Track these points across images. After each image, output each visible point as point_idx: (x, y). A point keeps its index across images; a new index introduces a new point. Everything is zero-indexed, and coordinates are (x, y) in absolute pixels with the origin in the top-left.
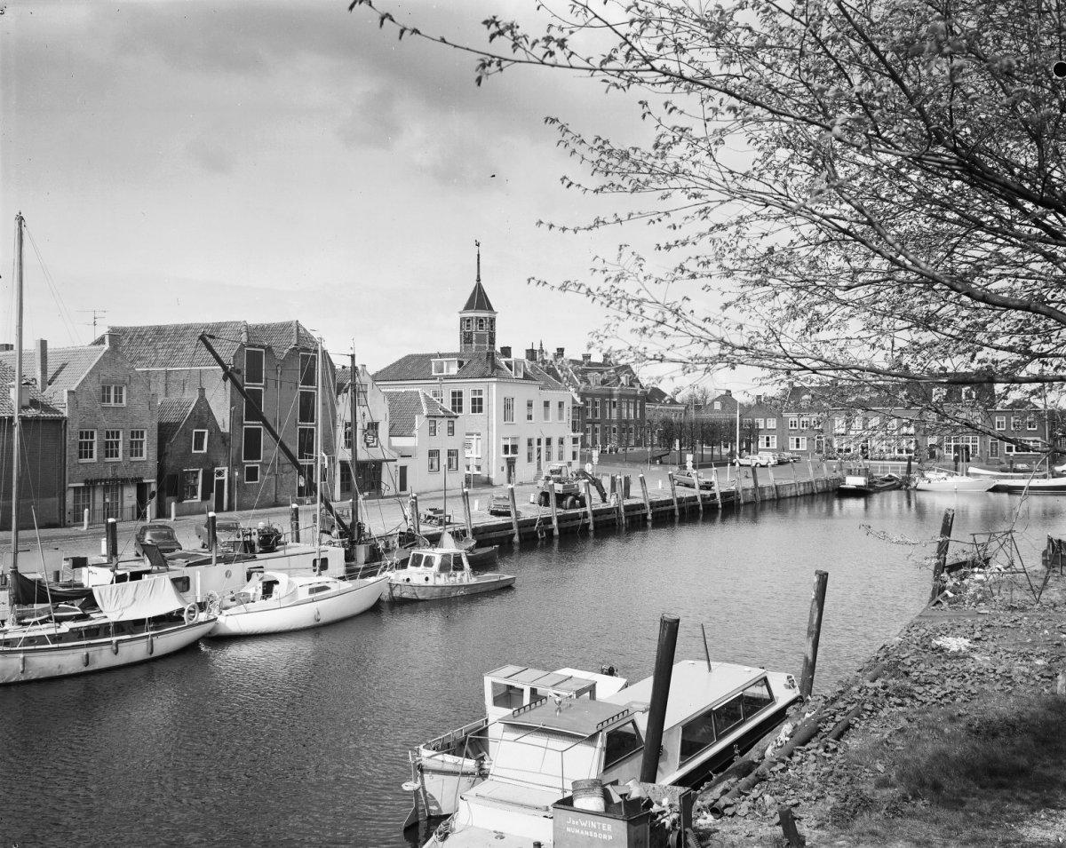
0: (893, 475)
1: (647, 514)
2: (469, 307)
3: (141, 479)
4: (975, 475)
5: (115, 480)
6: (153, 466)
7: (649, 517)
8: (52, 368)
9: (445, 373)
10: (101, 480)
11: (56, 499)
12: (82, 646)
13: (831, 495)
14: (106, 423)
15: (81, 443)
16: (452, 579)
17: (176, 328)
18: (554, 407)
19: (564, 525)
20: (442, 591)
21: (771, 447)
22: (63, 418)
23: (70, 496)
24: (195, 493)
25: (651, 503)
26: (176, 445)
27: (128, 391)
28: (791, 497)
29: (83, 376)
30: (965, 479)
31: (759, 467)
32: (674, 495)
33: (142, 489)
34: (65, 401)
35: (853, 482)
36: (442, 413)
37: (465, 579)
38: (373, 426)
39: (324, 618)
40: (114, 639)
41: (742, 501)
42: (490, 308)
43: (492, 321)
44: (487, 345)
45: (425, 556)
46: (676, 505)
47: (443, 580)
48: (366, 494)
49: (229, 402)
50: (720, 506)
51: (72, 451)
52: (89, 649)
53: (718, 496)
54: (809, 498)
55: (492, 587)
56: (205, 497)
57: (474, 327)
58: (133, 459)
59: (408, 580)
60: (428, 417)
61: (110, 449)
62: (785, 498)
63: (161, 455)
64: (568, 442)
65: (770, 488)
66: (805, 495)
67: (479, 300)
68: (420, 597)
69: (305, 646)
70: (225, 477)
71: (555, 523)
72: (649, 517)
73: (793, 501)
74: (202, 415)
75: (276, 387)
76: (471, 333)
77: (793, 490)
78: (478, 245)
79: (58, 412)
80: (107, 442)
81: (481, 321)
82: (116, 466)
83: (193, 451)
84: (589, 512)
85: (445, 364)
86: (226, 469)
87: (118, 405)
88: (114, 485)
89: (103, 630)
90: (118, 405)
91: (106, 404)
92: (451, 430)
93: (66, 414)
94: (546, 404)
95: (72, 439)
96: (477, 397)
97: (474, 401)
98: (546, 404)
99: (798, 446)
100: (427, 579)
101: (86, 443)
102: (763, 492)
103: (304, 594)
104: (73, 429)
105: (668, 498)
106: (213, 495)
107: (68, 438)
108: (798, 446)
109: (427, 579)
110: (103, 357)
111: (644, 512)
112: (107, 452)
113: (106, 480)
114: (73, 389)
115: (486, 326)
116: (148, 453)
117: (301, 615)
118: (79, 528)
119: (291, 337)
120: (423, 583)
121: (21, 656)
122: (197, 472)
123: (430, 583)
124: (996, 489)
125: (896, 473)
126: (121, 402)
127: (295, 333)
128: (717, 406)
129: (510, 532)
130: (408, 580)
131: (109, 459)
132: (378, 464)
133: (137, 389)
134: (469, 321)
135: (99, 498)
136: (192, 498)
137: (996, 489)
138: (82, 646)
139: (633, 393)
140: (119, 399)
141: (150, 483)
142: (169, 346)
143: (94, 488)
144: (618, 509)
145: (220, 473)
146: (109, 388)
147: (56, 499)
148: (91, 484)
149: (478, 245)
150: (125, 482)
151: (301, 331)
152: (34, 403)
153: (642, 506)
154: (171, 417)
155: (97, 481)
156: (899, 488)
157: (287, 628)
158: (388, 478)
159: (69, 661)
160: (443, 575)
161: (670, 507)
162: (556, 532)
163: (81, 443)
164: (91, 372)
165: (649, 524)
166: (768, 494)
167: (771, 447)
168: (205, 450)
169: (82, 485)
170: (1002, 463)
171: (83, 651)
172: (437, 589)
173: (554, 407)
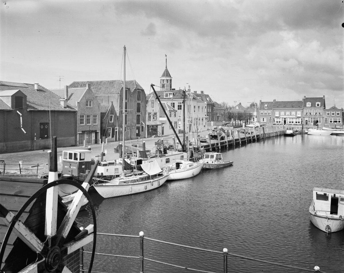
0: (298, 130)
1: (239, 142)
2: (163, 76)
3: (96, 131)
4: (325, 130)
5: (89, 131)
6: (99, 126)
7: (240, 143)
8: (69, 95)
9: (168, 97)
10: (86, 131)
11: (74, 137)
12: (144, 183)
13: (274, 137)
14: (87, 113)
15: (81, 119)
16: (219, 162)
17: (97, 82)
18: (197, 107)
19: (222, 145)
20: (217, 166)
21: (264, 121)
22: (77, 111)
23: (78, 136)
24: (109, 135)
25: (247, 137)
26: (106, 120)
27: (93, 102)
28: (272, 137)
29: (81, 98)
30: (323, 131)
31: (253, 128)
32: (239, 137)
33: (96, 133)
34: (77, 106)
35: (289, 132)
36: (173, 110)
37: (222, 162)
38: (155, 114)
39: (195, 174)
40: (152, 180)
41: (261, 138)
42: (170, 76)
43: (171, 80)
44: (169, 88)
45: (210, 155)
46: (246, 139)
47: (216, 163)
48: (155, 136)
49: (119, 106)
50: (256, 139)
51: (78, 122)
52: (146, 184)
53: (256, 136)
54: (276, 137)
55: (229, 165)
56: (113, 137)
57: (165, 82)
58: (94, 124)
59: (208, 162)
60: (169, 111)
61: (88, 121)
62: (271, 137)
63: (102, 123)
64: (204, 119)
65: (267, 134)
66: (275, 136)
67: (167, 73)
68: (211, 168)
69: (190, 182)
70: (118, 130)
71: (219, 145)
72: (240, 143)
73: (273, 138)
74: (112, 111)
75: (131, 101)
76: (164, 84)
77: (273, 135)
78: (166, 56)
79: (74, 109)
80: (87, 119)
81: (168, 80)
82: (90, 126)
83: (110, 122)
84: (227, 141)
85: (168, 94)
86: (118, 127)
87: (90, 107)
88: (90, 132)
89: (148, 178)
90: (90, 107)
91: (87, 107)
92: (175, 115)
93: (77, 110)
94: (199, 107)
95: (78, 118)
96: (180, 105)
97: (178, 106)
98: (199, 107)
99: (263, 120)
100: (213, 162)
101: (82, 119)
102: (265, 135)
103: (188, 167)
104: (79, 114)
105: (244, 137)
106: (115, 136)
107: (77, 117)
108: (263, 120)
109: (213, 162)
110: (87, 91)
111: (239, 141)
112: (81, 122)
113: (87, 131)
114: (79, 101)
115: (169, 82)
116: (98, 123)
117: (189, 174)
118: (82, 147)
119: (134, 85)
120: (211, 163)
121: (131, 186)
122: (110, 129)
123: (213, 163)
124: (332, 134)
125: (299, 129)
126: (91, 106)
127: (135, 84)
128: (237, 108)
129: (209, 147)
130: (208, 162)
131: (88, 124)
132: (157, 126)
133: (95, 101)
134: (163, 80)
135: (86, 137)
136: (109, 137)
137: (332, 134)
138: (144, 183)
139: (211, 104)
140: (90, 105)
141: (98, 132)
142: (96, 88)
143: (84, 134)
144: (233, 140)
145: (117, 129)
146: (88, 101)
147: (74, 137)
148: (84, 132)
149: (166, 56)
150: (92, 131)
151: (137, 83)
152: (68, 107)
153: (238, 140)
154: (103, 111)
155: (85, 131)
156: (300, 134)
157: (187, 177)
158: (159, 129)
159: (140, 188)
160: (216, 161)
161: (244, 140)
162: (220, 148)
163: (81, 119)
164: (83, 96)
165: (240, 145)
166: (267, 136)
167: (264, 121)
168: (113, 122)
169: (81, 132)
170: (328, 126)
171: (145, 185)
172: (216, 166)
173: (201, 108)
